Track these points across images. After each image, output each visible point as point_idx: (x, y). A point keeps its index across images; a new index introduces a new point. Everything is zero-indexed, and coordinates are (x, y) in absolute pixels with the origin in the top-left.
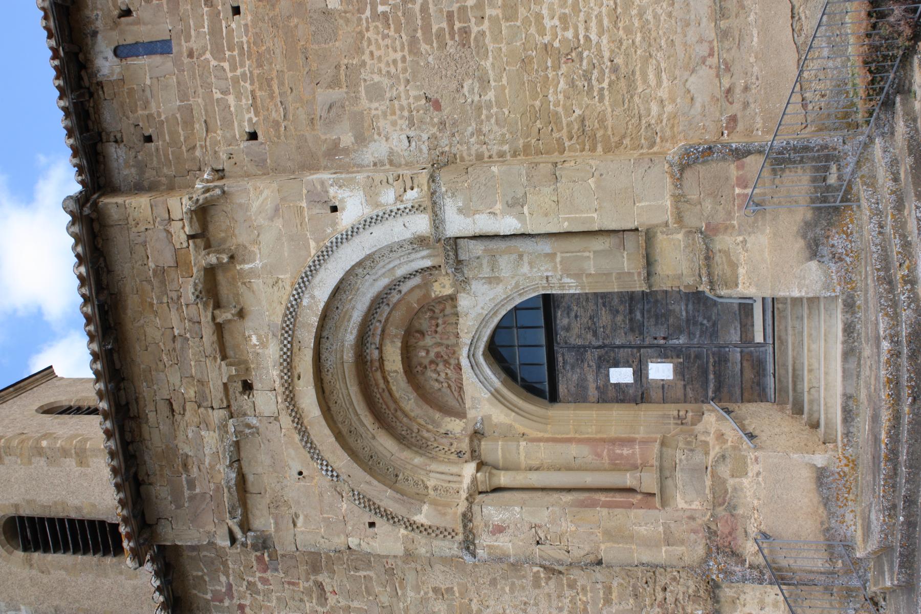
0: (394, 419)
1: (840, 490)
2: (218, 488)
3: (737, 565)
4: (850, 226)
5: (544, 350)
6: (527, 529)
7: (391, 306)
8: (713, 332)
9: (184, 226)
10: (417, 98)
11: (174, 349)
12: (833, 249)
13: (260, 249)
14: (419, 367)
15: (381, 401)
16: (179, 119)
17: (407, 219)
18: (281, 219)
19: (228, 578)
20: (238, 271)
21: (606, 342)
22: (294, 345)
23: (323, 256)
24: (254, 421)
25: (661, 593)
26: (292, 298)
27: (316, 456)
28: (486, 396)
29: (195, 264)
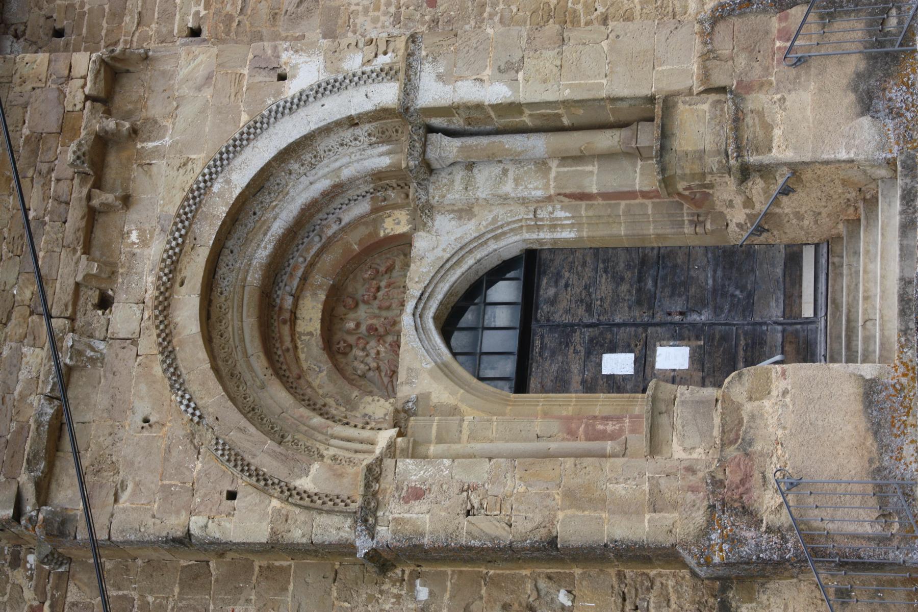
1: (895, 410)
2: (22, 428)
3: (749, 528)
4: (912, 76)
6: (457, 491)
7: (323, 240)
8: (748, 306)
12: (890, 103)
13: (174, 124)
14: (342, 342)
16: (107, 10)
17: (371, 88)
18: (212, 88)
20: (138, 150)
21: (603, 319)
22: (187, 241)
23: (255, 128)
24: (101, 346)
26: (201, 178)
27: (177, 386)
28: (429, 366)
29: (85, 128)
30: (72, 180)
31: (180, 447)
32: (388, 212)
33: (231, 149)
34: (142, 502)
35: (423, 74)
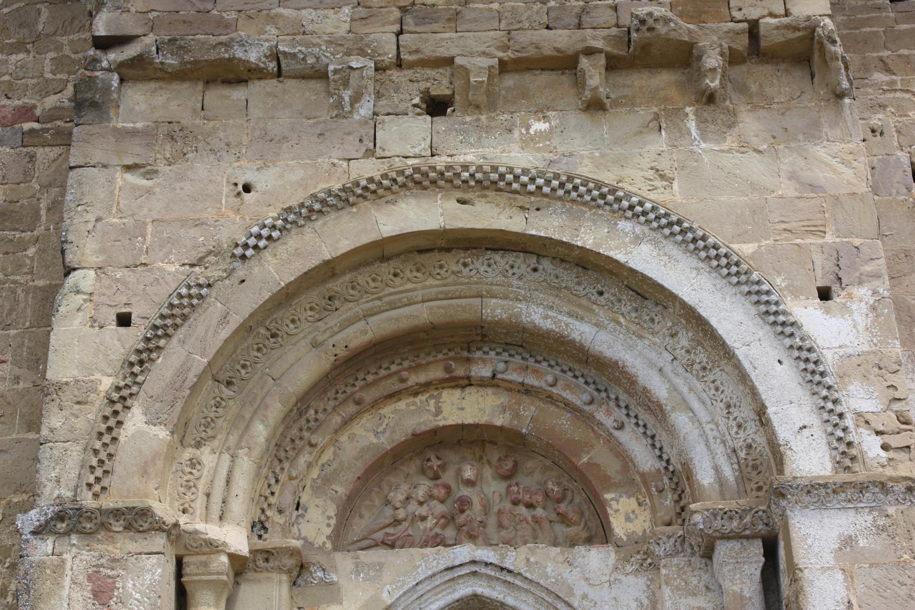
0: (341, 396)
7: (587, 408)
9: (776, 16)
13: (729, 151)
14: (439, 463)
15: (383, 372)
17: (818, 432)
18: (797, 194)
22: (533, 199)
24: (365, 109)
26: (635, 199)
27: (291, 217)
28: (385, 595)
30: (617, 26)
31: (202, 239)
32: (648, 501)
33: (690, 235)
34: (121, 202)
35: (852, 513)
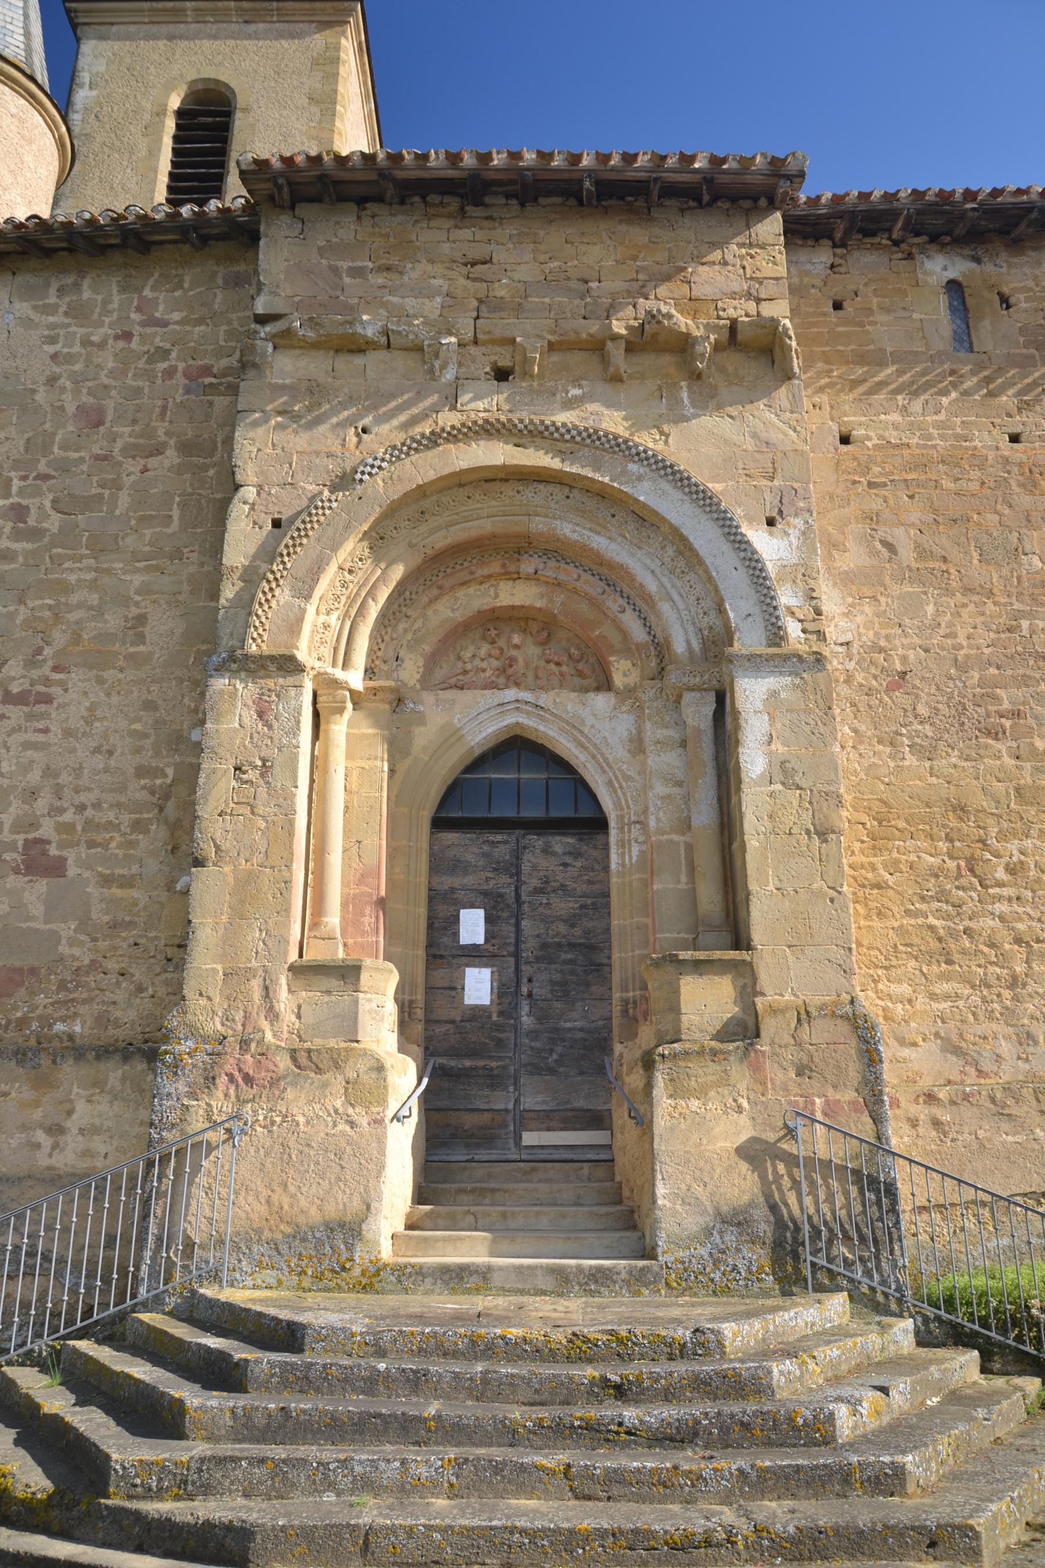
2: (351, 309)
5: (510, 813)
10: (904, 659)
11: (568, 279)
19: (177, 323)
21: (526, 907)
25: (117, 967)
30: (635, 319)
